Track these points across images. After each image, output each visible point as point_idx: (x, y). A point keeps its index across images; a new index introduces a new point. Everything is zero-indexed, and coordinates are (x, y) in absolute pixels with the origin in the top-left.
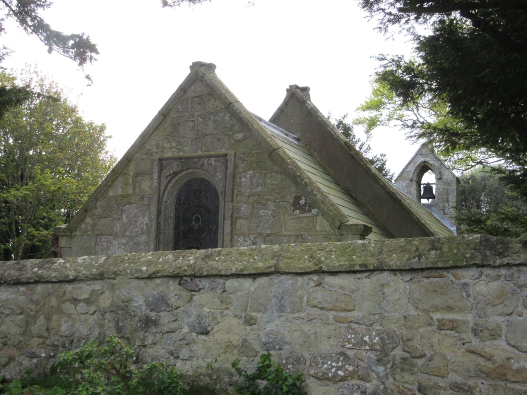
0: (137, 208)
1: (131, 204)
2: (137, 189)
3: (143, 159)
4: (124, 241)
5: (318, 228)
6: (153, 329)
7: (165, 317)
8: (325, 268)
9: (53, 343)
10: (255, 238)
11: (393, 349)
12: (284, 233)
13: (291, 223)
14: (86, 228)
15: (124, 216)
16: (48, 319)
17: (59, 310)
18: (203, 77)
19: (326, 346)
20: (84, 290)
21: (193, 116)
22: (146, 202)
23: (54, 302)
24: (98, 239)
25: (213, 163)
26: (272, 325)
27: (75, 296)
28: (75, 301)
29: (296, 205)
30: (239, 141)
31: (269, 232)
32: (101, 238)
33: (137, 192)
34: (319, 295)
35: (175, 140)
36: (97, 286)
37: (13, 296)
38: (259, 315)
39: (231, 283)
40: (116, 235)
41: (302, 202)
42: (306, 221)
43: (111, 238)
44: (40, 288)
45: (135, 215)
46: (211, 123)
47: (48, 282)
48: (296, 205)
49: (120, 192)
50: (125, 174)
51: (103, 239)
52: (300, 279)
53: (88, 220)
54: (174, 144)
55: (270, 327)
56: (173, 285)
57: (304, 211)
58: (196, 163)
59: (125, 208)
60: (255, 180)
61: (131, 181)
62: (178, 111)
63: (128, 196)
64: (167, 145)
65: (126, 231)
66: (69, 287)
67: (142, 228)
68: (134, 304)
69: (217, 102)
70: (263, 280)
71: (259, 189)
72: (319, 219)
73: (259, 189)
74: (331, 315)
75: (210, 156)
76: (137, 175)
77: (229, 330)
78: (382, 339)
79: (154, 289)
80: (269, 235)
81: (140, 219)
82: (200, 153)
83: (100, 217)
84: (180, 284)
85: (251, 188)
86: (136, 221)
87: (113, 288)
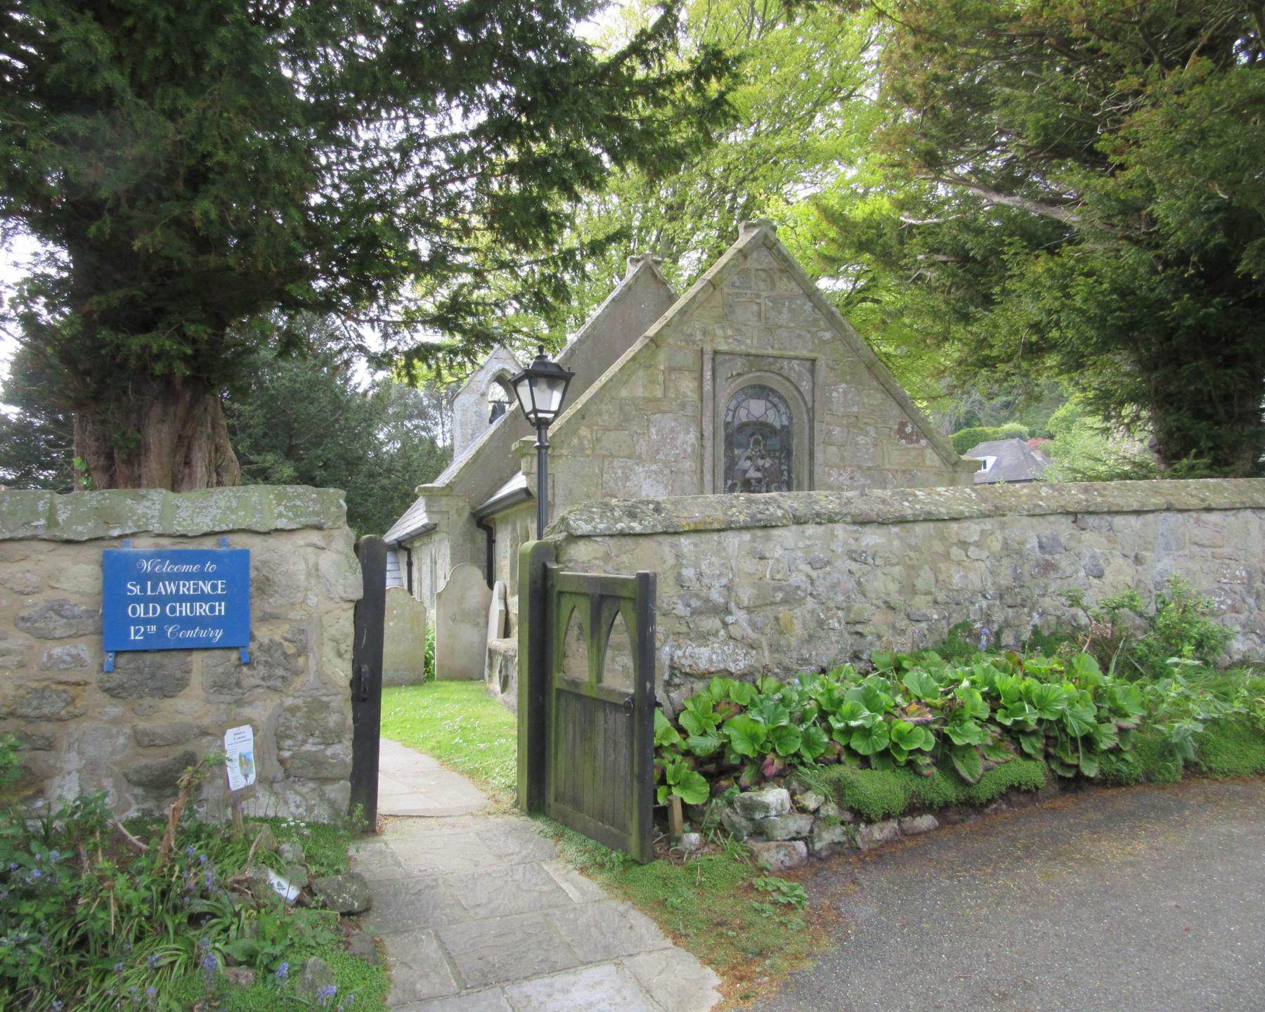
0: (675, 420)
1: (664, 412)
2: (672, 390)
3: (680, 348)
4: (654, 467)
5: (928, 463)
6: (1052, 575)
7: (1064, 563)
8: (1213, 506)
9: (307, 657)
10: (852, 472)
11: (894, 609)
12: (888, 466)
13: (896, 455)
14: (581, 443)
15: (653, 430)
16: (935, 571)
17: (947, 556)
18: (775, 244)
19: (1205, 583)
20: (972, 531)
21: (758, 296)
22: (689, 411)
23: (938, 547)
24: (606, 462)
25: (796, 368)
26: (1164, 565)
27: (962, 538)
28: (963, 544)
29: (901, 432)
30: (825, 342)
31: (870, 464)
32: (611, 462)
33: (672, 394)
34: (1198, 533)
35: (731, 327)
36: (988, 525)
37: (883, 540)
38: (1148, 554)
39: (1118, 521)
40: (640, 457)
41: (909, 429)
42: (913, 453)
43: (630, 462)
44: (919, 529)
45: (672, 430)
46: (785, 310)
47: (938, 520)
48: (901, 432)
49: (640, 392)
50: (649, 367)
51: (615, 463)
52: (1179, 516)
53: (584, 432)
54: (730, 332)
55: (1160, 566)
56: (1066, 522)
57: (911, 442)
58: (770, 364)
59: (653, 418)
60: (850, 396)
61: (661, 378)
62: (733, 285)
63: (655, 400)
64: (719, 332)
65: (657, 452)
66: (954, 526)
67: (685, 451)
68: (1028, 546)
69: (793, 284)
70: (1150, 517)
71: (855, 409)
72: (929, 452)
73: (855, 409)
74: (1209, 551)
75: (791, 358)
76: (671, 369)
77: (1120, 575)
78: (1248, 572)
79: (1046, 528)
80: (869, 468)
81: (681, 436)
82: (770, 351)
83: (606, 429)
84: (1074, 522)
85: (845, 407)
86: (673, 439)
87: (1003, 526)
